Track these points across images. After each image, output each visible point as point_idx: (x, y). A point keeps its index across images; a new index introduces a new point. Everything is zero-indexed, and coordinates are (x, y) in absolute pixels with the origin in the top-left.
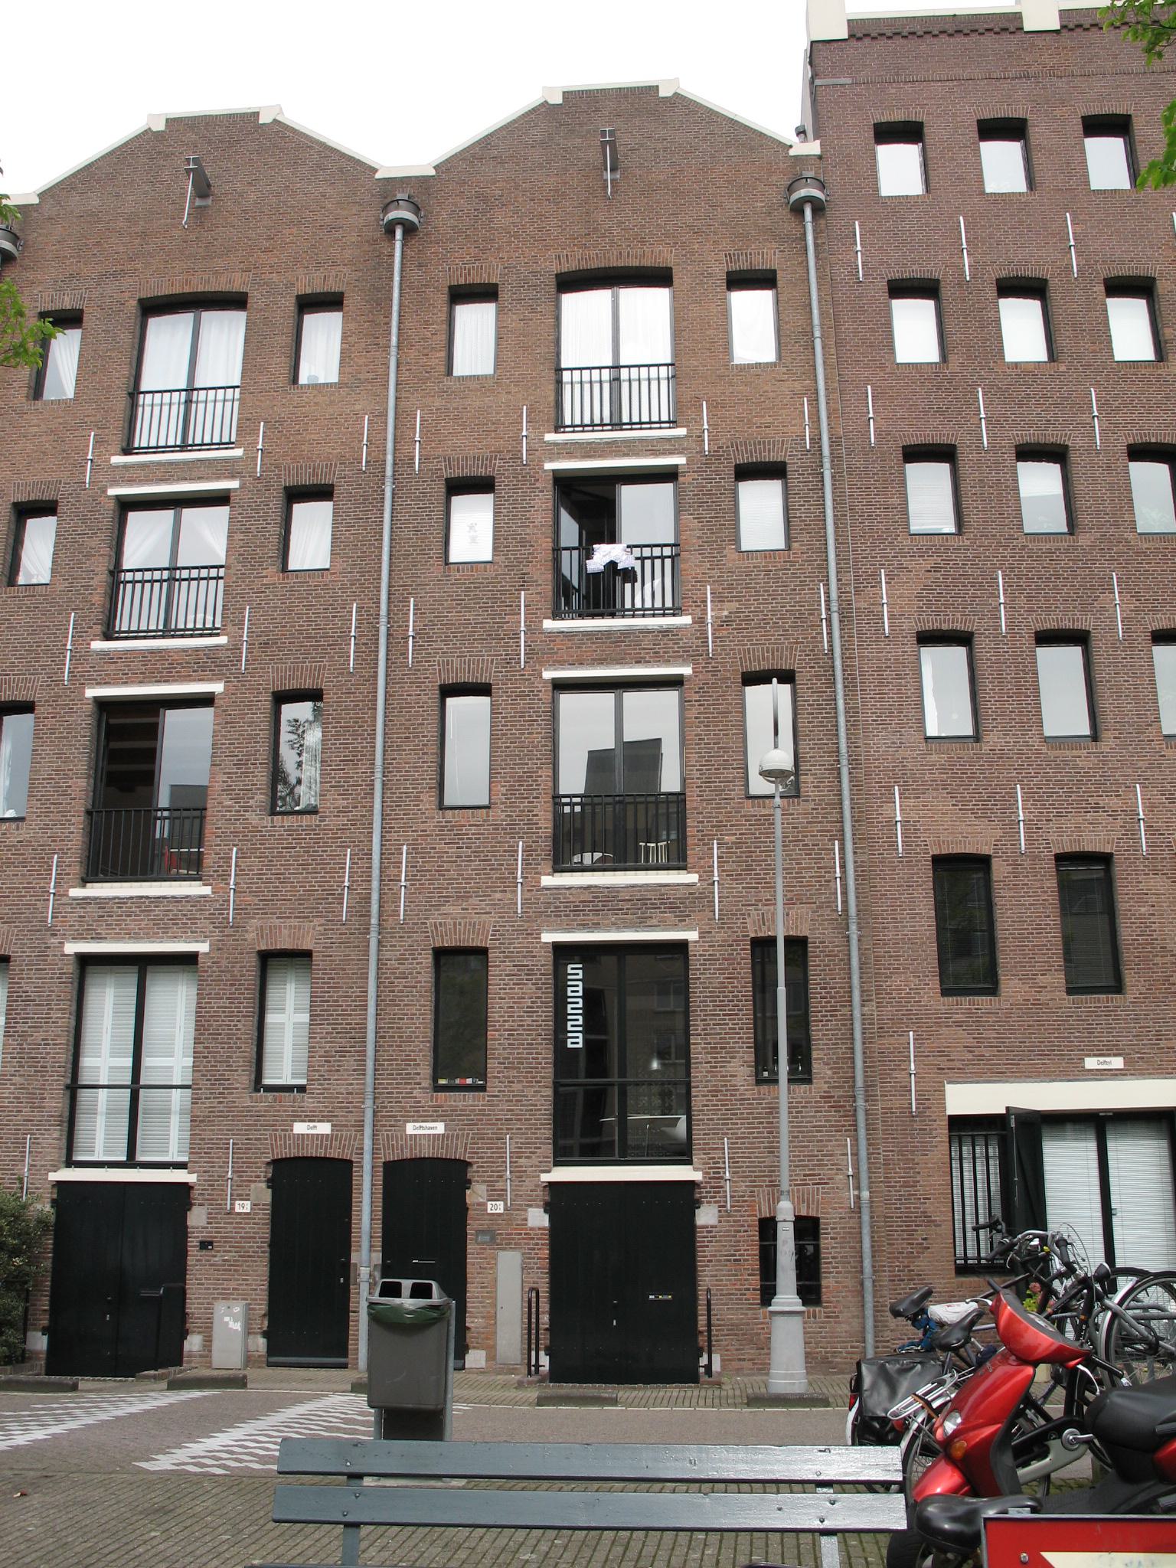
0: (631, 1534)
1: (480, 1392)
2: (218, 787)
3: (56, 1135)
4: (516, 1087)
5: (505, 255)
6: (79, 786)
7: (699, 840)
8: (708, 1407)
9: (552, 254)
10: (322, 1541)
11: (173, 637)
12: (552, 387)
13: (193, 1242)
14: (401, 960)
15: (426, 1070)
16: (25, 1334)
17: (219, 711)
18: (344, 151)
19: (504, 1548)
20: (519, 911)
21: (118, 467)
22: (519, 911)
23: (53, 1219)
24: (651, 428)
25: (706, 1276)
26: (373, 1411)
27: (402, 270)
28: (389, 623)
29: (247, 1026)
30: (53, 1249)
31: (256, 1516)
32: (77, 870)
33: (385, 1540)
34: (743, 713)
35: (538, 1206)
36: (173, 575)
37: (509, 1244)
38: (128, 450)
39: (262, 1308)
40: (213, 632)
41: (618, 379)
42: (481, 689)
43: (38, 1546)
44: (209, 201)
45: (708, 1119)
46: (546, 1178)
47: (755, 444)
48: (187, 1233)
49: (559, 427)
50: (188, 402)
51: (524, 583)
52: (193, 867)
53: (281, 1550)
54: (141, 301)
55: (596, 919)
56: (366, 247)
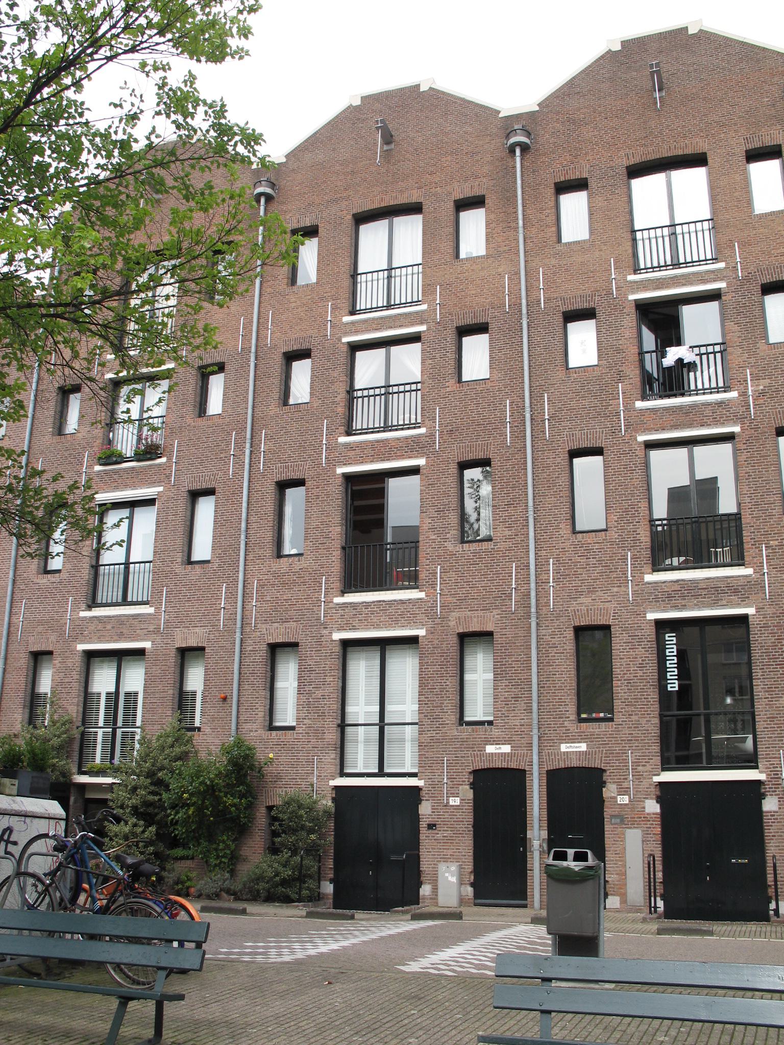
0: (735, 1028)
1: (617, 925)
2: (425, 527)
3: (333, 756)
4: (634, 718)
5: (591, 158)
6: (336, 531)
7: (752, 545)
8: (779, 939)
9: (622, 153)
10: (522, 1021)
11: (390, 431)
12: (630, 244)
13: (423, 825)
14: (553, 635)
15: (572, 708)
16: (319, 883)
17: (424, 477)
18: (477, 102)
19: (646, 1032)
20: (631, 599)
21: (347, 324)
22: (631, 599)
23: (333, 810)
24: (700, 265)
25: (772, 846)
26: (550, 936)
27: (522, 176)
28: (531, 411)
29: (452, 683)
30: (335, 829)
31: (477, 1003)
32: (338, 585)
33: (564, 1023)
34: (778, 455)
35: (652, 799)
36: (387, 390)
37: (633, 824)
38: (353, 312)
39: (469, 867)
40: (416, 426)
41: (674, 234)
42: (597, 451)
43: (342, 1015)
44: (392, 146)
45: (768, 738)
46: (657, 779)
47: (774, 268)
48: (419, 818)
49: (636, 270)
50: (389, 277)
51: (621, 377)
52: (412, 580)
53: (496, 1026)
54: (354, 215)
55: (683, 602)
56: (497, 163)
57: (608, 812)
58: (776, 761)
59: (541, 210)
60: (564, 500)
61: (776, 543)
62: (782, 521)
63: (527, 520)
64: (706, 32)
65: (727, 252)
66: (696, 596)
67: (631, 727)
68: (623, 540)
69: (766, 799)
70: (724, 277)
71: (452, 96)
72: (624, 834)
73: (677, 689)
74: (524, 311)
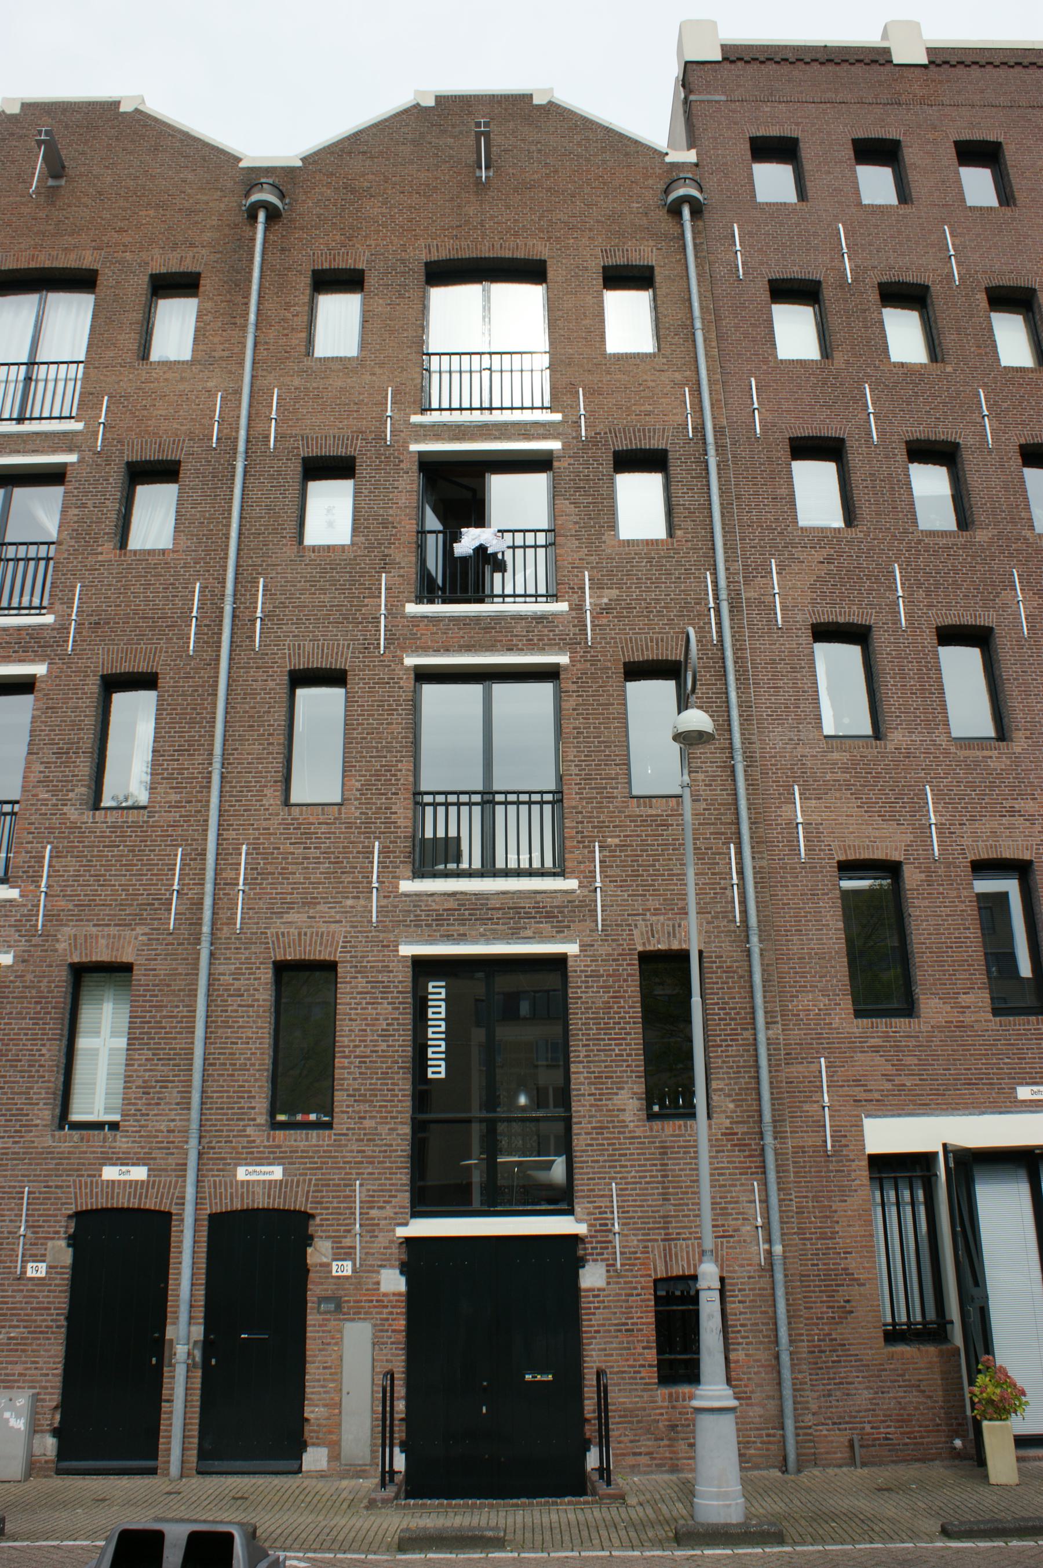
4: (368, 1123)
9: (422, 242)
14: (237, 975)
15: (261, 1104)
18: (207, 140)
20: (374, 920)
22: (374, 920)
35: (392, 1267)
37: (358, 1314)
39: (53, 1398)
44: (63, 182)
45: (593, 1161)
46: (402, 1232)
51: (386, 564)
56: (227, 231)
57: (314, 1291)
58: (603, 1203)
59: (288, 306)
60: (275, 749)
61: (617, 841)
62: (627, 807)
63: (209, 779)
64: (558, 106)
65: (567, 399)
66: (484, 921)
67: (362, 1140)
68: (368, 823)
69: (587, 1267)
70: (559, 434)
71: (169, 126)
72: (341, 1332)
73: (443, 1076)
74: (241, 447)
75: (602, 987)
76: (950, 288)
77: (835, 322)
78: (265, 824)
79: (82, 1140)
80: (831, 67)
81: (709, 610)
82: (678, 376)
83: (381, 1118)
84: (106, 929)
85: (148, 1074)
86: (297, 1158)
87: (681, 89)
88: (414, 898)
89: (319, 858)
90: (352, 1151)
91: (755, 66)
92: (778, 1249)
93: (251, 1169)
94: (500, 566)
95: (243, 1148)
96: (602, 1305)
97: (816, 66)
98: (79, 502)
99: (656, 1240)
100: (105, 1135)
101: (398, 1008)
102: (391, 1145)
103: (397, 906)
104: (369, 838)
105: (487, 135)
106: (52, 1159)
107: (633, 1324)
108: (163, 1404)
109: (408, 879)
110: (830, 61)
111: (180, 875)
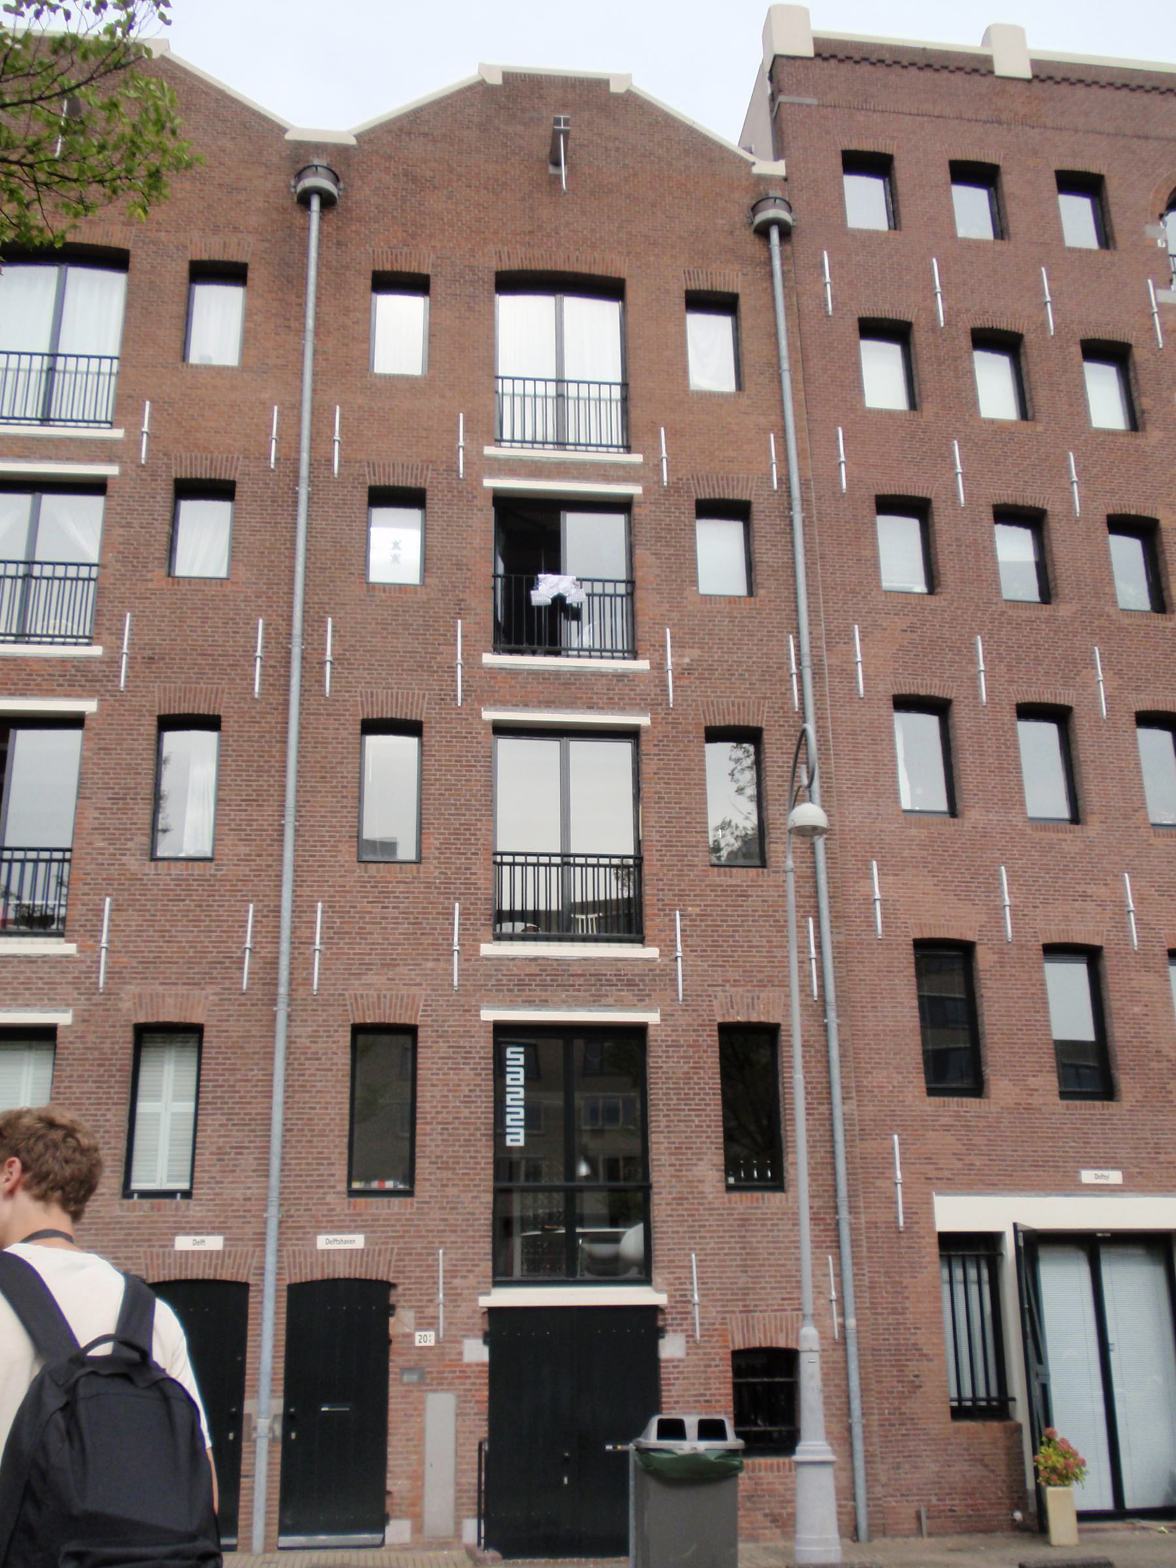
4: (452, 1191)
14: (314, 1037)
20: (456, 983)
22: (456, 983)
35: (475, 1337)
37: (440, 1383)
46: (486, 1301)
51: (461, 610)
56: (275, 215)
57: (396, 1362)
58: (680, 1273)
61: (697, 910)
66: (565, 987)
68: (447, 883)
72: (423, 1402)
73: (521, 1143)
74: (304, 471)
75: (683, 1057)
76: (1045, 339)
77: (924, 370)
78: (340, 881)
79: (152, 1208)
80: (928, 74)
81: (791, 676)
82: (762, 420)
83: (464, 1185)
84: (173, 987)
85: (222, 1140)
86: (379, 1226)
87: (768, 83)
88: (496, 962)
89: (397, 918)
90: (434, 1220)
91: (849, 65)
92: (851, 1322)
93: (331, 1237)
94: (575, 614)
95: (324, 1216)
96: (681, 1376)
97: (913, 71)
98: (123, 521)
99: (733, 1312)
100: (177, 1205)
101: (480, 1074)
102: (474, 1214)
103: (477, 970)
104: (449, 898)
105: (566, 134)
106: (121, 1229)
107: (711, 1395)
108: (242, 1480)
109: (489, 942)
110: (929, 66)
111: (253, 932)
